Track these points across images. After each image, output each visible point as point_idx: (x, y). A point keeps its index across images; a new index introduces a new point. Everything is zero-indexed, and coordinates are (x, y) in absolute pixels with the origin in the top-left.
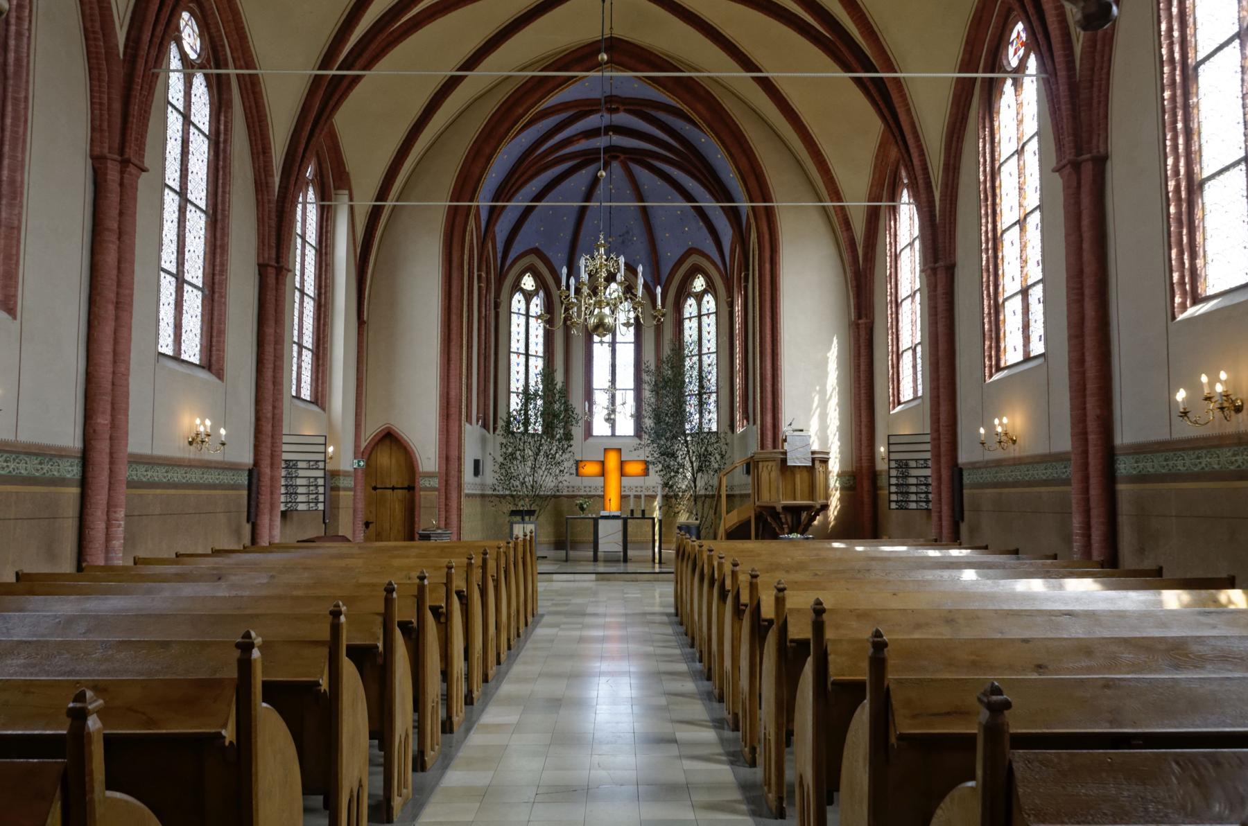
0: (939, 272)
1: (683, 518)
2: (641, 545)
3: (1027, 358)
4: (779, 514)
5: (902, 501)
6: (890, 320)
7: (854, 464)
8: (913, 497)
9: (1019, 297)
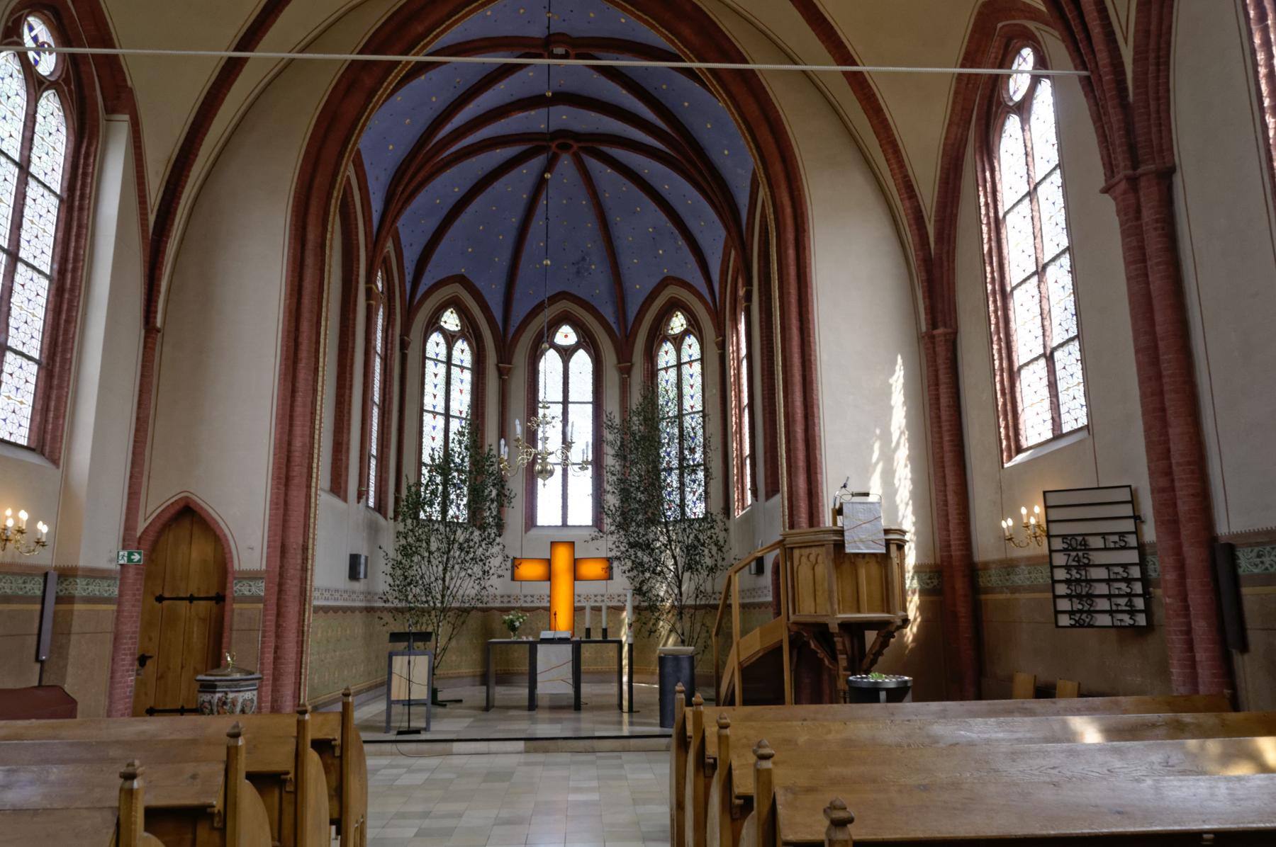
0: (1143, 183)
1: (670, 644)
2: (601, 677)
3: (1058, 435)
4: (832, 635)
5: (1081, 611)
6: (993, 320)
7: (938, 555)
8: (1103, 604)
9: (1042, 362)
